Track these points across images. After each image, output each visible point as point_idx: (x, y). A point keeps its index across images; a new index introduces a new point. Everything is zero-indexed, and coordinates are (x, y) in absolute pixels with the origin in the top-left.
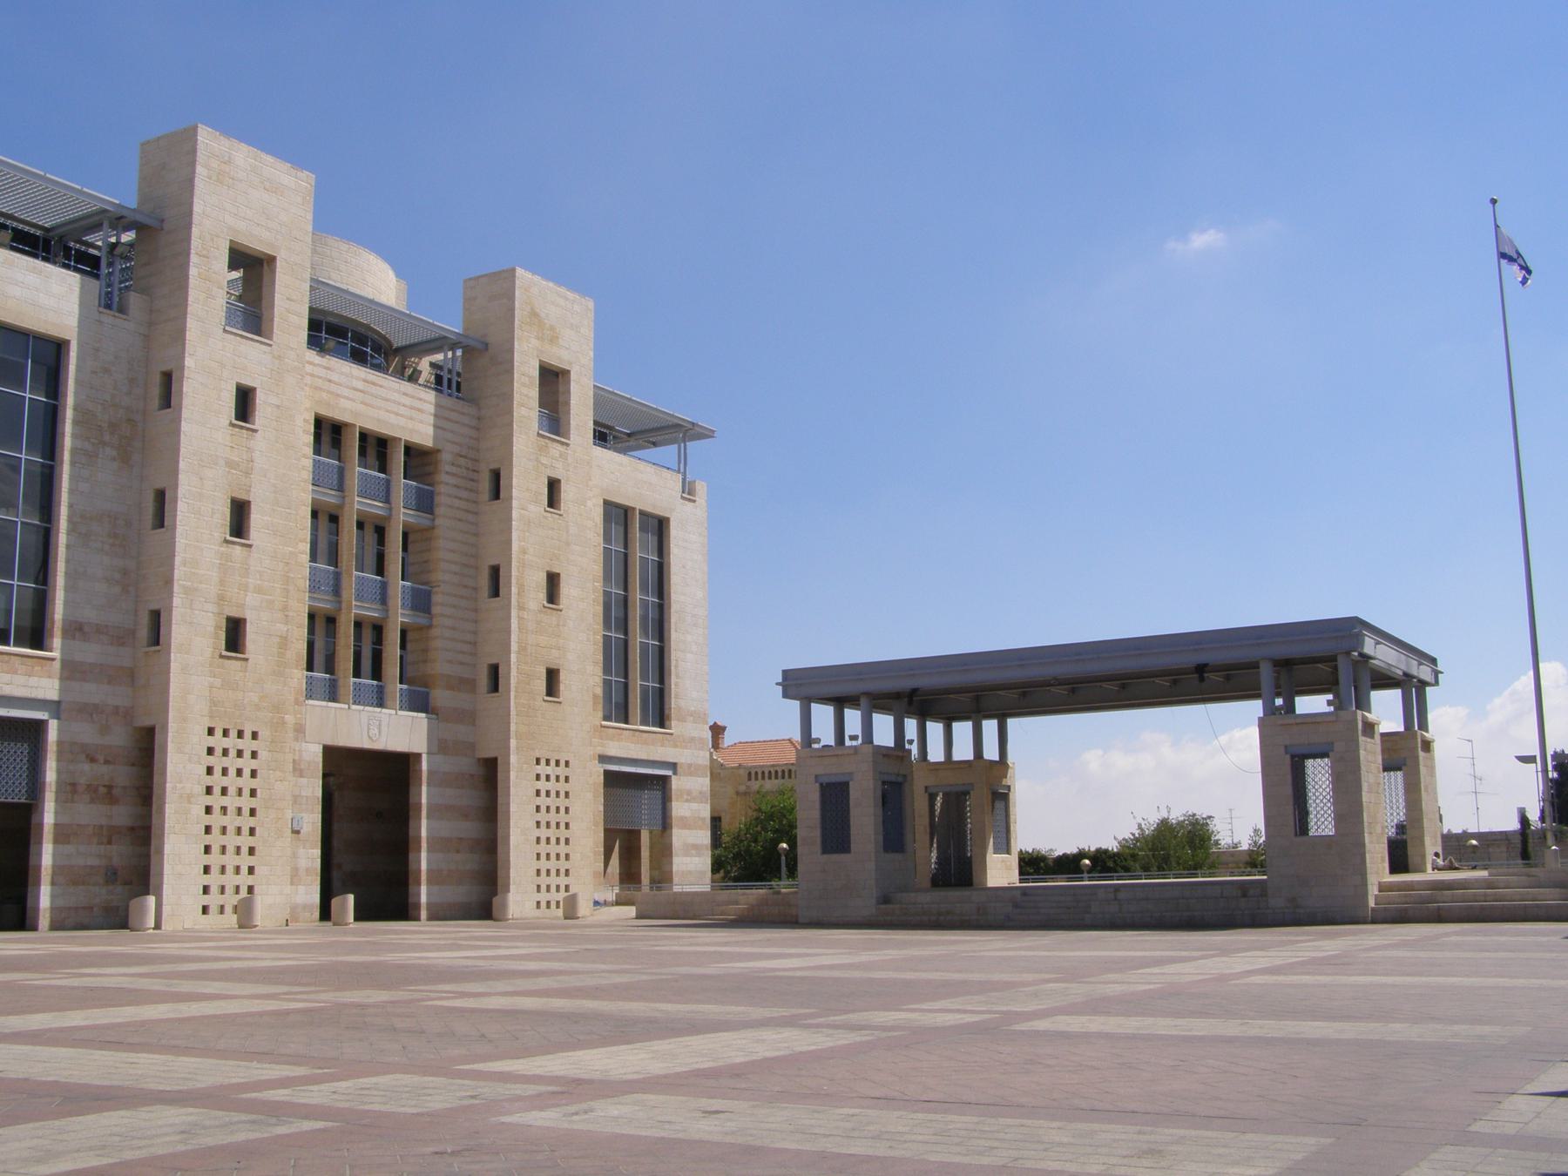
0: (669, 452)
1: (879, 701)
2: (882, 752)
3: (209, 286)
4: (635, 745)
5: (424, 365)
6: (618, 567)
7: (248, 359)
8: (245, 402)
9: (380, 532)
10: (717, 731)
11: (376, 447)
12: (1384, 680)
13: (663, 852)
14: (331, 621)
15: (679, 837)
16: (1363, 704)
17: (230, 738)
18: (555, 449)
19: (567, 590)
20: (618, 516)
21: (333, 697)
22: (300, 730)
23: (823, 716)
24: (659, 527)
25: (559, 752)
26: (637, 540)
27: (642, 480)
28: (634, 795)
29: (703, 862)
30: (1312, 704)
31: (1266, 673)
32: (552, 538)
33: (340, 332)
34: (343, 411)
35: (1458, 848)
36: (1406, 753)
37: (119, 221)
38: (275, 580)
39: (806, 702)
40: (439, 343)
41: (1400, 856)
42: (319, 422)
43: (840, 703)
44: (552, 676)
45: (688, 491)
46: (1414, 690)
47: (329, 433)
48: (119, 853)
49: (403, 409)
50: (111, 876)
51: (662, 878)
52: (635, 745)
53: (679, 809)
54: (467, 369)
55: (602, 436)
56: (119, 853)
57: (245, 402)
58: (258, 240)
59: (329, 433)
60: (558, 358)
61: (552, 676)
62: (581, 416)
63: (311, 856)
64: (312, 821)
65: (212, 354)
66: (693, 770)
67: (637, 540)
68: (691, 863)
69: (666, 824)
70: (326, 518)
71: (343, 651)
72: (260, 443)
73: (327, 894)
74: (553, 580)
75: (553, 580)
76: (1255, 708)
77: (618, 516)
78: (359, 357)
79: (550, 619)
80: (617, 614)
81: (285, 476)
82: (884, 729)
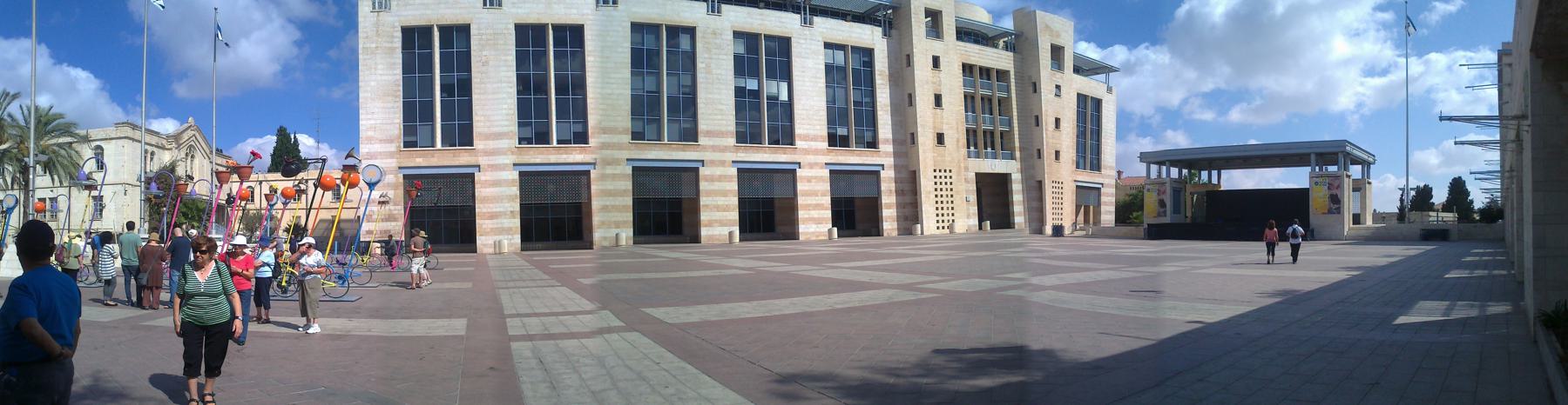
0: (1102, 77)
1: (1174, 163)
2: (1175, 181)
3: (919, 24)
4: (1087, 177)
5: (1001, 43)
6: (1081, 116)
7: (936, 47)
8: (936, 62)
9: (990, 100)
10: (1119, 173)
11: (985, 72)
12: (1356, 161)
13: (1098, 213)
14: (975, 131)
15: (1103, 208)
16: (1346, 169)
17: (941, 172)
18: (1059, 75)
19: (1062, 124)
20: (1082, 98)
21: (978, 156)
22: (966, 169)
23: (1154, 168)
24: (1098, 103)
25: (1063, 176)
26: (1089, 110)
27: (1092, 86)
28: (1087, 197)
29: (1112, 217)
30: (1333, 169)
31: (1313, 157)
32: (1058, 100)
33: (967, 33)
34: (973, 60)
35: (1378, 217)
36: (1360, 187)
37: (886, 7)
38: (954, 118)
39: (1149, 164)
40: (1006, 34)
41: (1357, 219)
42: (964, 65)
43: (1160, 163)
44: (1057, 153)
45: (1109, 90)
46: (1366, 165)
47: (967, 69)
48: (908, 211)
49: (997, 58)
50: (906, 219)
51: (1097, 221)
52: (1087, 177)
53: (1103, 199)
54: (1020, 42)
55: (1077, 70)
56: (908, 211)
57: (936, 62)
58: (935, 6)
59: (967, 69)
60: (1059, 42)
61: (1057, 153)
62: (1069, 63)
63: (974, 209)
64: (973, 198)
65: (922, 47)
66: (1109, 186)
67: (1089, 110)
68: (1108, 216)
69: (1099, 204)
70: (969, 99)
71: (979, 141)
72: (945, 114)
73: (981, 221)
74: (1057, 121)
75: (1057, 121)
76: (1309, 169)
77: (1082, 98)
78: (976, 42)
79: (1057, 133)
80: (1081, 134)
81: (953, 85)
82: (1174, 172)
